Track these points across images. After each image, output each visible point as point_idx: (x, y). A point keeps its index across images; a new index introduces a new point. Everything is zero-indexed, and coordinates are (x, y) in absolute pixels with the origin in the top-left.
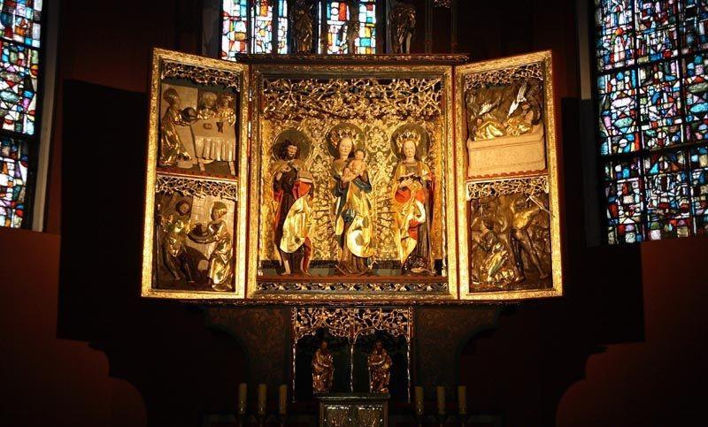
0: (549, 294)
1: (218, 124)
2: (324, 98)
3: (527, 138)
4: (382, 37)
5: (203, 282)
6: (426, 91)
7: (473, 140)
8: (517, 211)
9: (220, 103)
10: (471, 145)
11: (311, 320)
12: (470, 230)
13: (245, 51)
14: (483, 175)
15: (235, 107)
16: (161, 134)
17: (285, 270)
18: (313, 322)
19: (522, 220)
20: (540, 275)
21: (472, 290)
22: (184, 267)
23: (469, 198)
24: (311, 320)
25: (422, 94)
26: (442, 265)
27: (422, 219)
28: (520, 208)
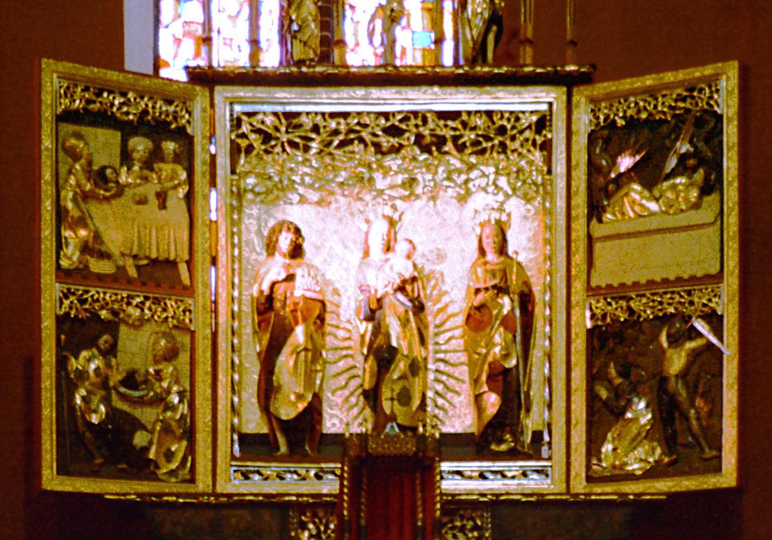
0: (710, 482)
1: (158, 195)
2: (342, 144)
3: (695, 217)
4: (71, 77)
5: (140, 465)
6: (521, 132)
7: (600, 221)
8: (670, 344)
9: (155, 156)
10: (598, 230)
11: (322, 528)
12: (592, 379)
13: (202, 62)
14: (672, 278)
15: (186, 164)
16: (727, 193)
17: (278, 449)
18: (325, 532)
19: (676, 361)
20: (702, 450)
21: (590, 479)
22: (110, 445)
23: (589, 324)
24: (322, 528)
25: (513, 138)
26: (542, 439)
27: (512, 363)
28: (675, 341)
